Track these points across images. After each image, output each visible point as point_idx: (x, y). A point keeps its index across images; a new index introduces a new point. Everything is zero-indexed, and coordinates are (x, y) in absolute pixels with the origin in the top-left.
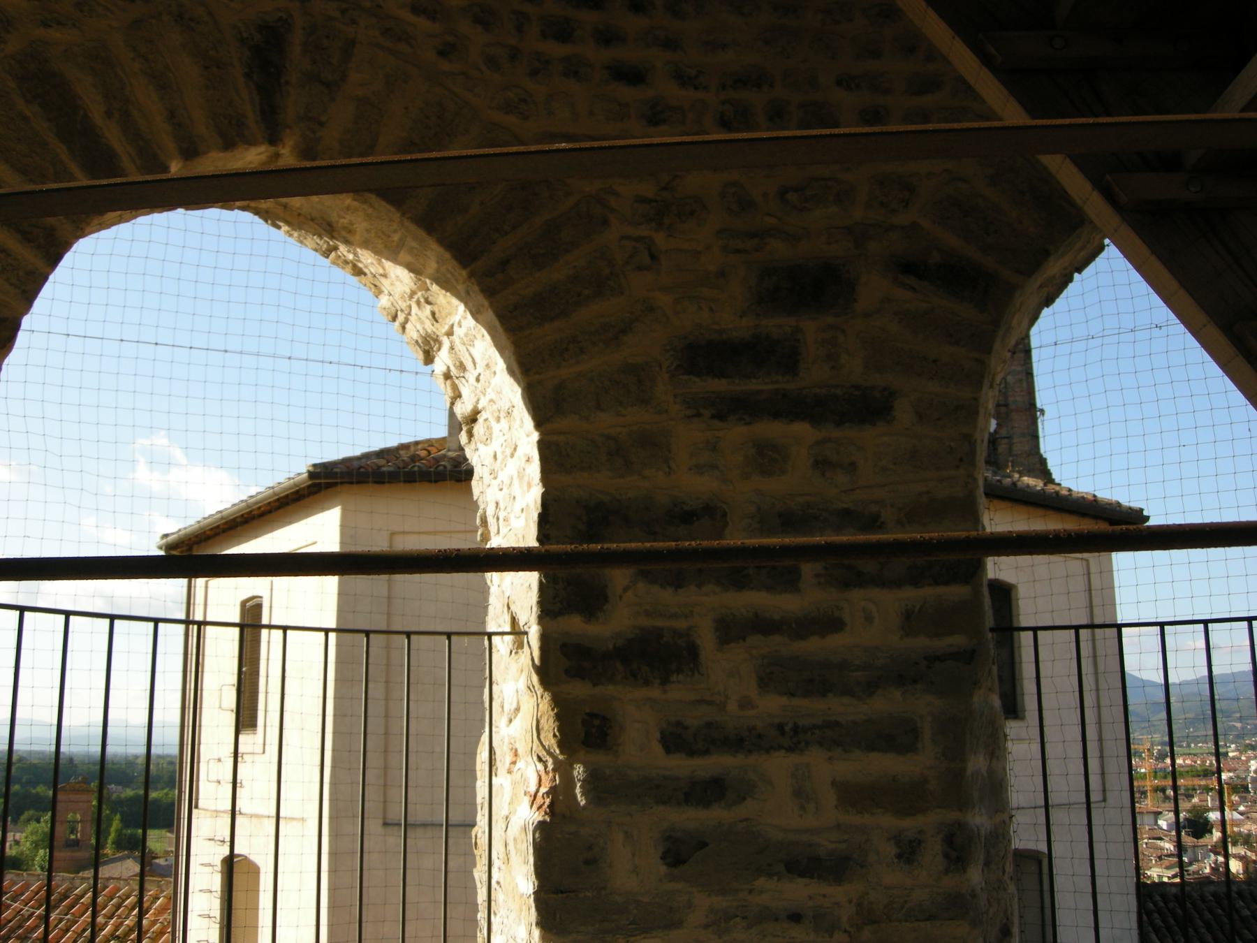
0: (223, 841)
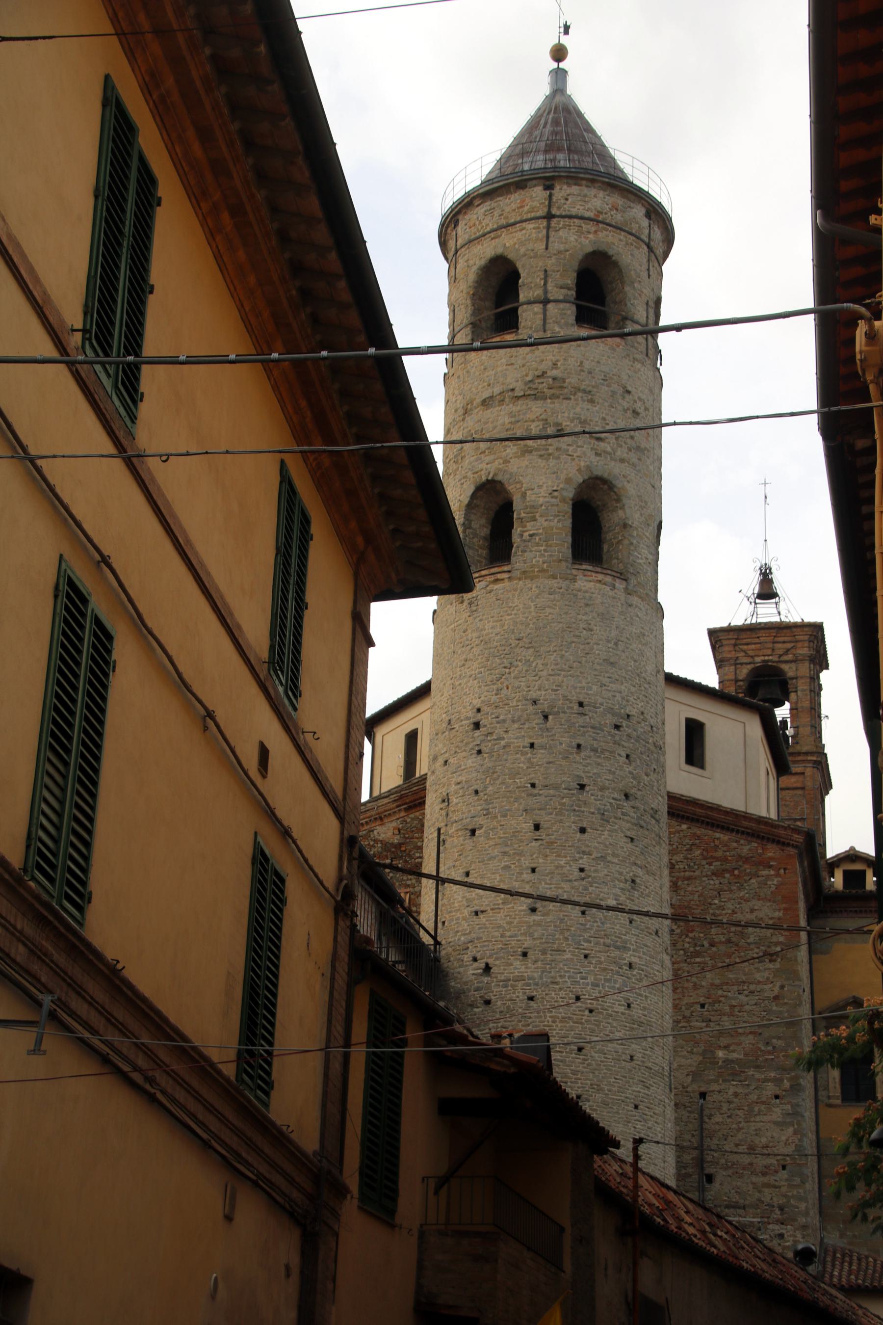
0: (767, 591)
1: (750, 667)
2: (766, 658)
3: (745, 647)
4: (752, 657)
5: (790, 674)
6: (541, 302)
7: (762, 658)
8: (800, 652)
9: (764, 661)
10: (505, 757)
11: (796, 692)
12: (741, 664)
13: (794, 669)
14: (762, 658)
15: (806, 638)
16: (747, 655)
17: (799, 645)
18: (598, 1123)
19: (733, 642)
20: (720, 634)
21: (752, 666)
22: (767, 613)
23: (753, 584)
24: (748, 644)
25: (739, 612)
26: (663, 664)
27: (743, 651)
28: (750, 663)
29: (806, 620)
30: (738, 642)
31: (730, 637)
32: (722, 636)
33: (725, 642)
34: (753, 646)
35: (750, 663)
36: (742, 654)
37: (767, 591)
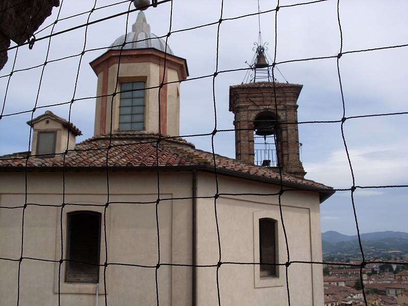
1: (257, 112)
2: (267, 107)
3: (254, 99)
4: (258, 106)
5: (283, 118)
6: (112, 138)
7: (265, 107)
8: (288, 104)
9: (265, 109)
10: (352, 295)
11: (287, 130)
12: (251, 110)
13: (284, 114)
14: (265, 107)
15: (292, 94)
16: (255, 105)
17: (288, 99)
18: (25, 36)
19: (246, 95)
20: (237, 90)
21: (258, 112)
22: (262, 76)
23: (252, 58)
24: (255, 97)
25: (244, 78)
26: (166, 133)
27: (253, 102)
28: (257, 110)
29: (290, 82)
30: (249, 96)
31: (245, 92)
32: (239, 91)
33: (240, 95)
34: (258, 99)
35: (257, 110)
36: (251, 104)
37: (260, 63)
